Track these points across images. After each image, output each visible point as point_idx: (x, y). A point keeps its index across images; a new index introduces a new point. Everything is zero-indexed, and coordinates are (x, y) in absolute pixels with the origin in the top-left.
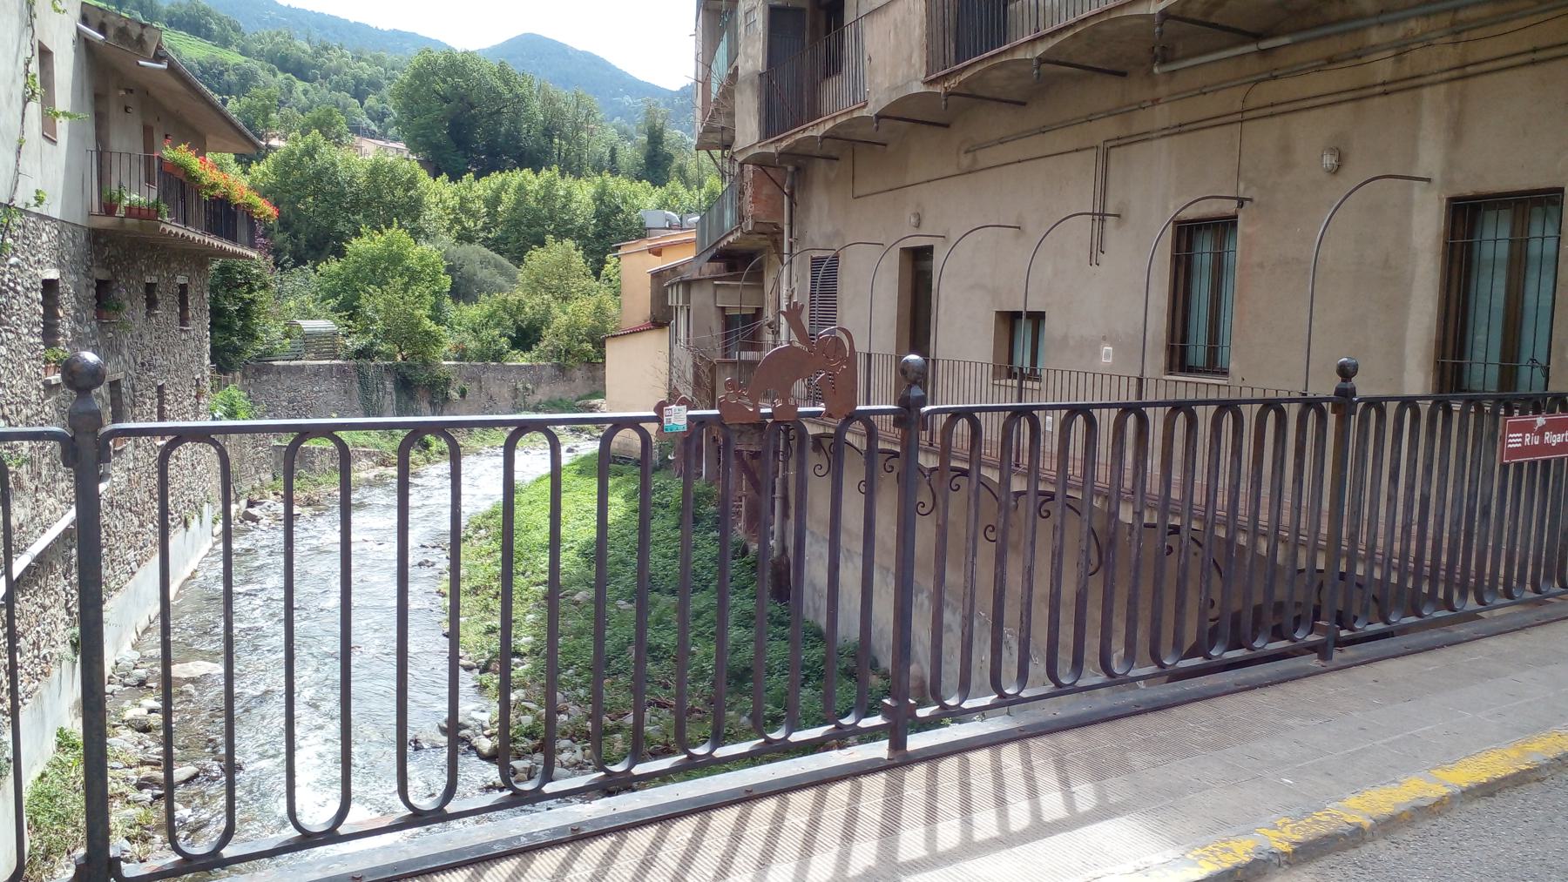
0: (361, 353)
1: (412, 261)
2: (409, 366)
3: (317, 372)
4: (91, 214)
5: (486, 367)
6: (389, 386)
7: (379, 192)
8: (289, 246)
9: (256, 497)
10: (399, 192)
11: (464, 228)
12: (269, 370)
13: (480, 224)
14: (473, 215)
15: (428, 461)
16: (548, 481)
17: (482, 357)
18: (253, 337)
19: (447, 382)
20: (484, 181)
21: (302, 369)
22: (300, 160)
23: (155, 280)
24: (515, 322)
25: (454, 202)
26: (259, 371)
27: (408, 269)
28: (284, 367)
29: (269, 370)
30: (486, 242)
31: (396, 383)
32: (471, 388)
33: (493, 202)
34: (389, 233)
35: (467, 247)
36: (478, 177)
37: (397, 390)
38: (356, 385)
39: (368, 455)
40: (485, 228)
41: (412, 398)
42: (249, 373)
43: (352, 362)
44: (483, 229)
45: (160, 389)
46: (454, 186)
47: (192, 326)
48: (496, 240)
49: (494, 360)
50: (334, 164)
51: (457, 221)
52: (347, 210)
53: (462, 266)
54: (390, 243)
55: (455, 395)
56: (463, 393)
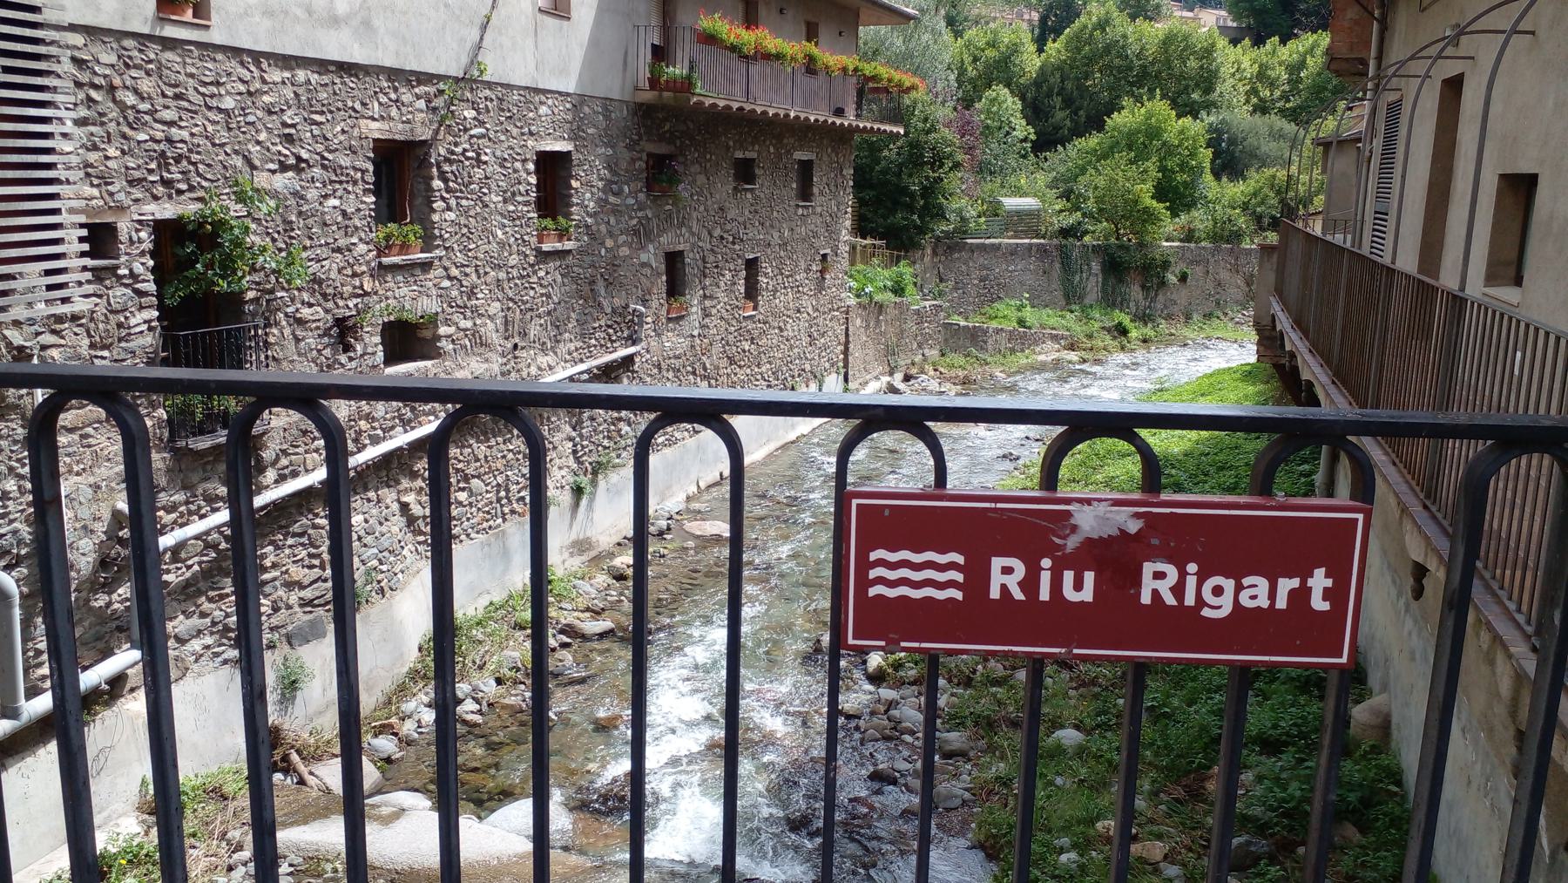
0: (1065, 233)
1: (1170, 136)
2: (1121, 247)
3: (1013, 251)
4: (637, 89)
5: (1217, 250)
6: (1096, 267)
7: (1168, 61)
8: (1068, 122)
9: (914, 371)
10: (1193, 63)
11: (1260, 100)
12: (961, 247)
13: (1277, 93)
14: (1272, 85)
15: (1123, 348)
16: (727, 488)
17: (1215, 237)
18: (941, 214)
19: (1166, 265)
20: (1291, 44)
21: (997, 247)
22: (1091, 35)
23: (754, 155)
24: (1282, 201)
25: (1250, 70)
26: (951, 249)
27: (1164, 144)
28: (978, 246)
29: (961, 247)
30: (1282, 112)
31: (1103, 265)
32: (1196, 272)
33: (1295, 68)
34: (1149, 105)
35: (1258, 119)
36: (1283, 42)
37: (1103, 271)
38: (1057, 266)
39: (1055, 338)
40: (1285, 97)
41: (1121, 281)
42: (940, 251)
43: (1055, 241)
44: (1280, 99)
45: (752, 266)
46: (1254, 53)
47: (819, 201)
48: (1294, 110)
49: (1228, 242)
50: (1125, 36)
51: (1254, 91)
52: (1132, 84)
53: (1245, 139)
54: (1149, 116)
55: (1172, 278)
56: (1183, 278)
